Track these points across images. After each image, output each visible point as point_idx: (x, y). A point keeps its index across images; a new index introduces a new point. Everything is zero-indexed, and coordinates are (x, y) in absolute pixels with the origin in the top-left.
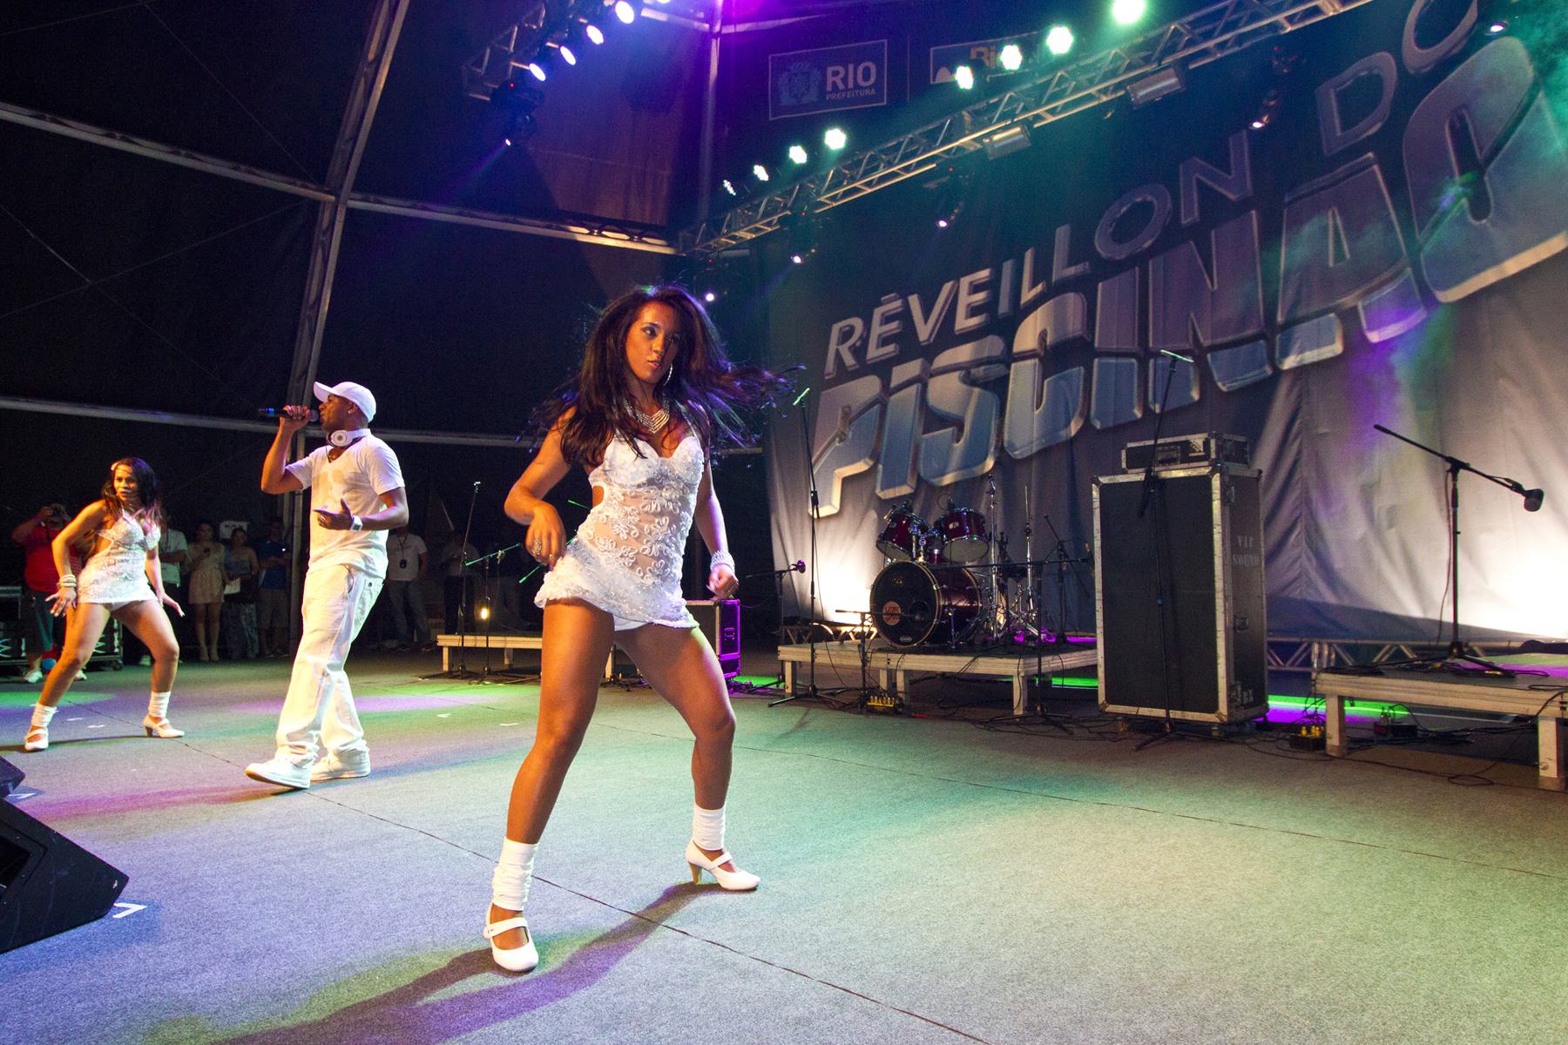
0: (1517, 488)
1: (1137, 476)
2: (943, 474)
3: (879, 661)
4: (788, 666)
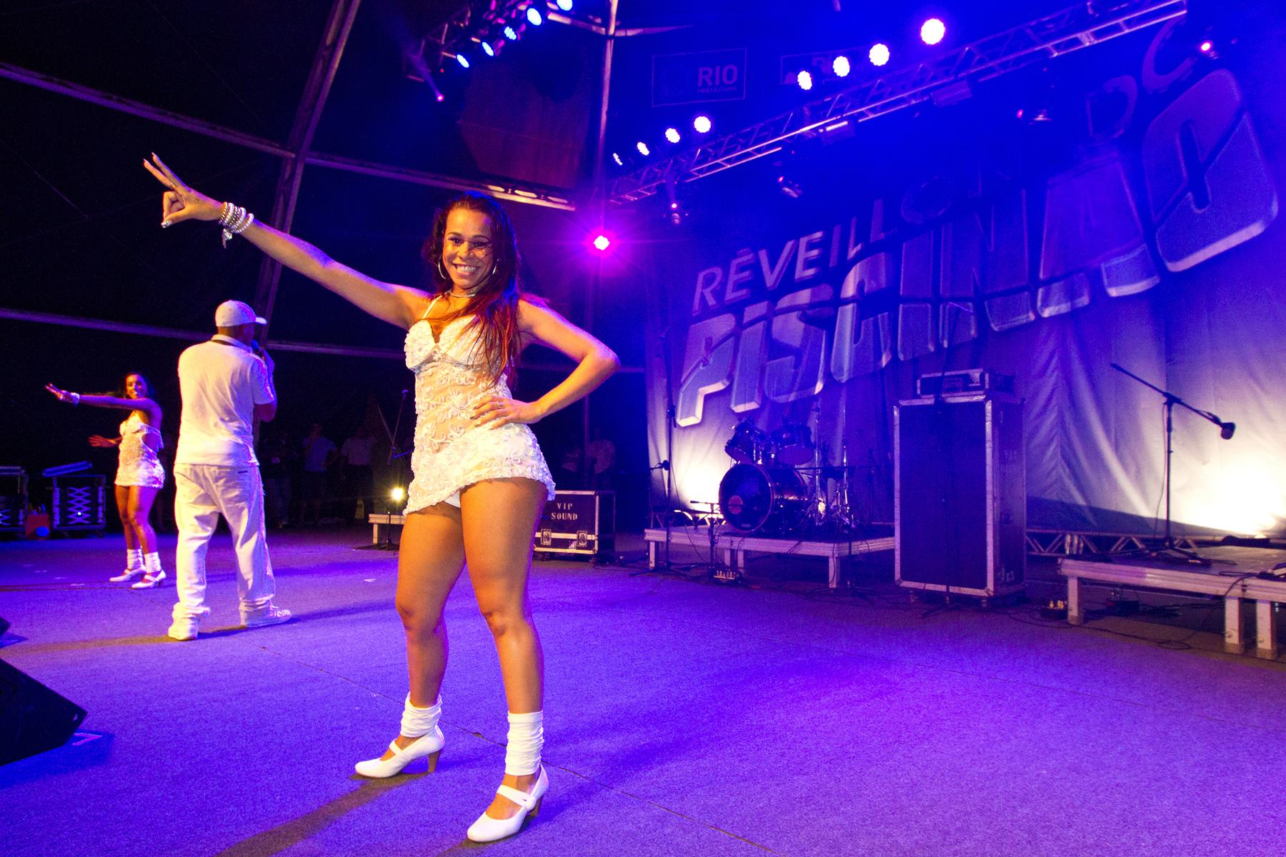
0: (1216, 420)
1: (929, 401)
3: (724, 542)
4: (652, 545)
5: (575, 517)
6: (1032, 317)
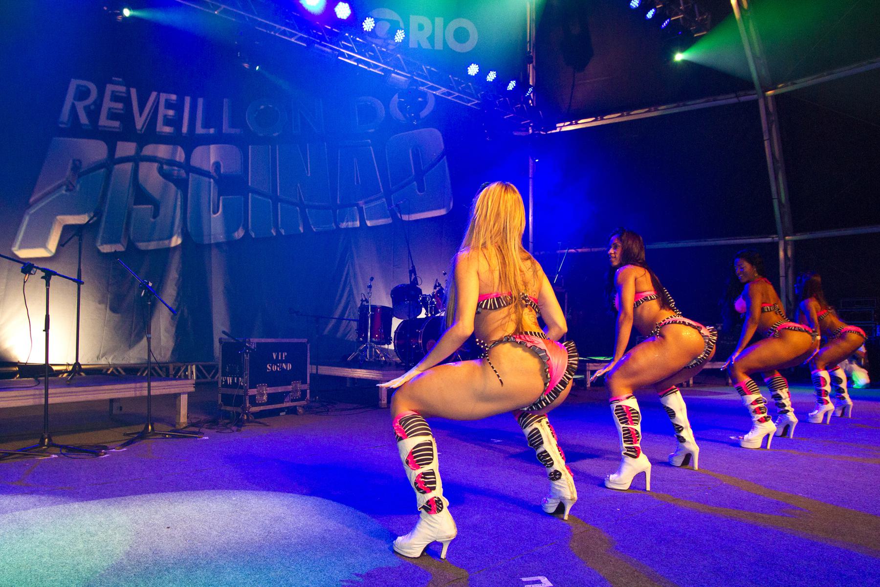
2: (170, 237)
5: (290, 366)
6: (358, 224)
